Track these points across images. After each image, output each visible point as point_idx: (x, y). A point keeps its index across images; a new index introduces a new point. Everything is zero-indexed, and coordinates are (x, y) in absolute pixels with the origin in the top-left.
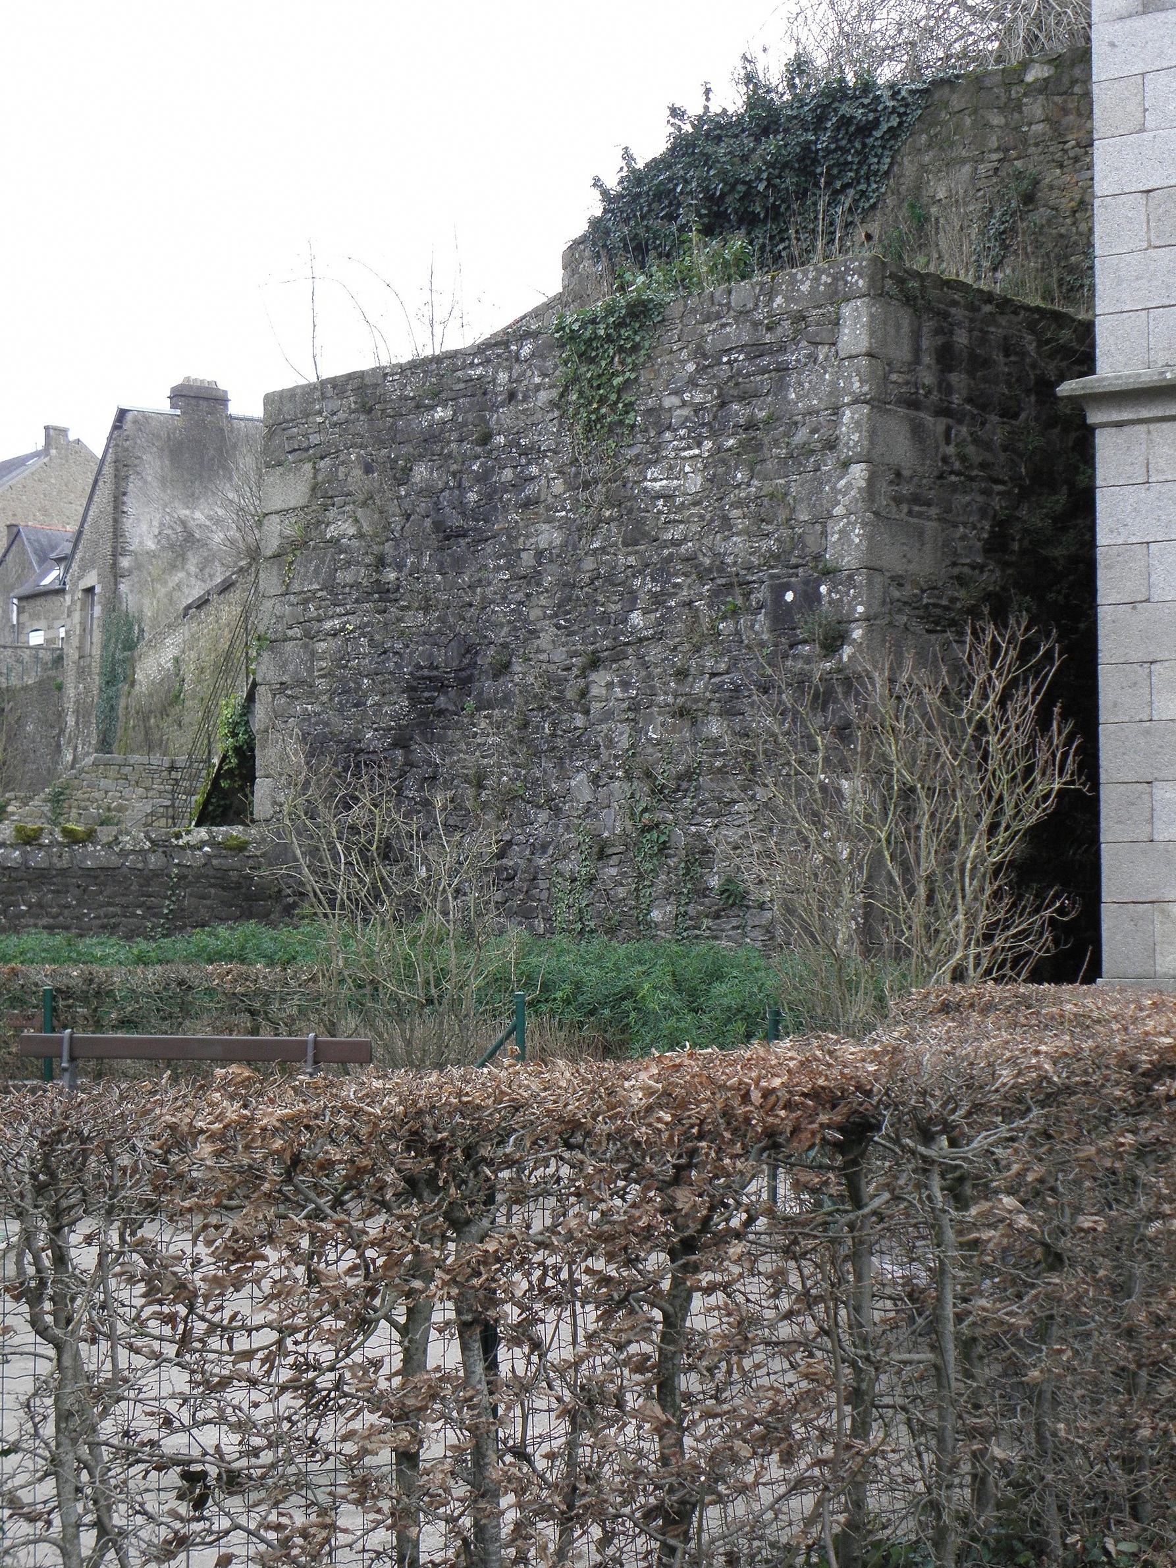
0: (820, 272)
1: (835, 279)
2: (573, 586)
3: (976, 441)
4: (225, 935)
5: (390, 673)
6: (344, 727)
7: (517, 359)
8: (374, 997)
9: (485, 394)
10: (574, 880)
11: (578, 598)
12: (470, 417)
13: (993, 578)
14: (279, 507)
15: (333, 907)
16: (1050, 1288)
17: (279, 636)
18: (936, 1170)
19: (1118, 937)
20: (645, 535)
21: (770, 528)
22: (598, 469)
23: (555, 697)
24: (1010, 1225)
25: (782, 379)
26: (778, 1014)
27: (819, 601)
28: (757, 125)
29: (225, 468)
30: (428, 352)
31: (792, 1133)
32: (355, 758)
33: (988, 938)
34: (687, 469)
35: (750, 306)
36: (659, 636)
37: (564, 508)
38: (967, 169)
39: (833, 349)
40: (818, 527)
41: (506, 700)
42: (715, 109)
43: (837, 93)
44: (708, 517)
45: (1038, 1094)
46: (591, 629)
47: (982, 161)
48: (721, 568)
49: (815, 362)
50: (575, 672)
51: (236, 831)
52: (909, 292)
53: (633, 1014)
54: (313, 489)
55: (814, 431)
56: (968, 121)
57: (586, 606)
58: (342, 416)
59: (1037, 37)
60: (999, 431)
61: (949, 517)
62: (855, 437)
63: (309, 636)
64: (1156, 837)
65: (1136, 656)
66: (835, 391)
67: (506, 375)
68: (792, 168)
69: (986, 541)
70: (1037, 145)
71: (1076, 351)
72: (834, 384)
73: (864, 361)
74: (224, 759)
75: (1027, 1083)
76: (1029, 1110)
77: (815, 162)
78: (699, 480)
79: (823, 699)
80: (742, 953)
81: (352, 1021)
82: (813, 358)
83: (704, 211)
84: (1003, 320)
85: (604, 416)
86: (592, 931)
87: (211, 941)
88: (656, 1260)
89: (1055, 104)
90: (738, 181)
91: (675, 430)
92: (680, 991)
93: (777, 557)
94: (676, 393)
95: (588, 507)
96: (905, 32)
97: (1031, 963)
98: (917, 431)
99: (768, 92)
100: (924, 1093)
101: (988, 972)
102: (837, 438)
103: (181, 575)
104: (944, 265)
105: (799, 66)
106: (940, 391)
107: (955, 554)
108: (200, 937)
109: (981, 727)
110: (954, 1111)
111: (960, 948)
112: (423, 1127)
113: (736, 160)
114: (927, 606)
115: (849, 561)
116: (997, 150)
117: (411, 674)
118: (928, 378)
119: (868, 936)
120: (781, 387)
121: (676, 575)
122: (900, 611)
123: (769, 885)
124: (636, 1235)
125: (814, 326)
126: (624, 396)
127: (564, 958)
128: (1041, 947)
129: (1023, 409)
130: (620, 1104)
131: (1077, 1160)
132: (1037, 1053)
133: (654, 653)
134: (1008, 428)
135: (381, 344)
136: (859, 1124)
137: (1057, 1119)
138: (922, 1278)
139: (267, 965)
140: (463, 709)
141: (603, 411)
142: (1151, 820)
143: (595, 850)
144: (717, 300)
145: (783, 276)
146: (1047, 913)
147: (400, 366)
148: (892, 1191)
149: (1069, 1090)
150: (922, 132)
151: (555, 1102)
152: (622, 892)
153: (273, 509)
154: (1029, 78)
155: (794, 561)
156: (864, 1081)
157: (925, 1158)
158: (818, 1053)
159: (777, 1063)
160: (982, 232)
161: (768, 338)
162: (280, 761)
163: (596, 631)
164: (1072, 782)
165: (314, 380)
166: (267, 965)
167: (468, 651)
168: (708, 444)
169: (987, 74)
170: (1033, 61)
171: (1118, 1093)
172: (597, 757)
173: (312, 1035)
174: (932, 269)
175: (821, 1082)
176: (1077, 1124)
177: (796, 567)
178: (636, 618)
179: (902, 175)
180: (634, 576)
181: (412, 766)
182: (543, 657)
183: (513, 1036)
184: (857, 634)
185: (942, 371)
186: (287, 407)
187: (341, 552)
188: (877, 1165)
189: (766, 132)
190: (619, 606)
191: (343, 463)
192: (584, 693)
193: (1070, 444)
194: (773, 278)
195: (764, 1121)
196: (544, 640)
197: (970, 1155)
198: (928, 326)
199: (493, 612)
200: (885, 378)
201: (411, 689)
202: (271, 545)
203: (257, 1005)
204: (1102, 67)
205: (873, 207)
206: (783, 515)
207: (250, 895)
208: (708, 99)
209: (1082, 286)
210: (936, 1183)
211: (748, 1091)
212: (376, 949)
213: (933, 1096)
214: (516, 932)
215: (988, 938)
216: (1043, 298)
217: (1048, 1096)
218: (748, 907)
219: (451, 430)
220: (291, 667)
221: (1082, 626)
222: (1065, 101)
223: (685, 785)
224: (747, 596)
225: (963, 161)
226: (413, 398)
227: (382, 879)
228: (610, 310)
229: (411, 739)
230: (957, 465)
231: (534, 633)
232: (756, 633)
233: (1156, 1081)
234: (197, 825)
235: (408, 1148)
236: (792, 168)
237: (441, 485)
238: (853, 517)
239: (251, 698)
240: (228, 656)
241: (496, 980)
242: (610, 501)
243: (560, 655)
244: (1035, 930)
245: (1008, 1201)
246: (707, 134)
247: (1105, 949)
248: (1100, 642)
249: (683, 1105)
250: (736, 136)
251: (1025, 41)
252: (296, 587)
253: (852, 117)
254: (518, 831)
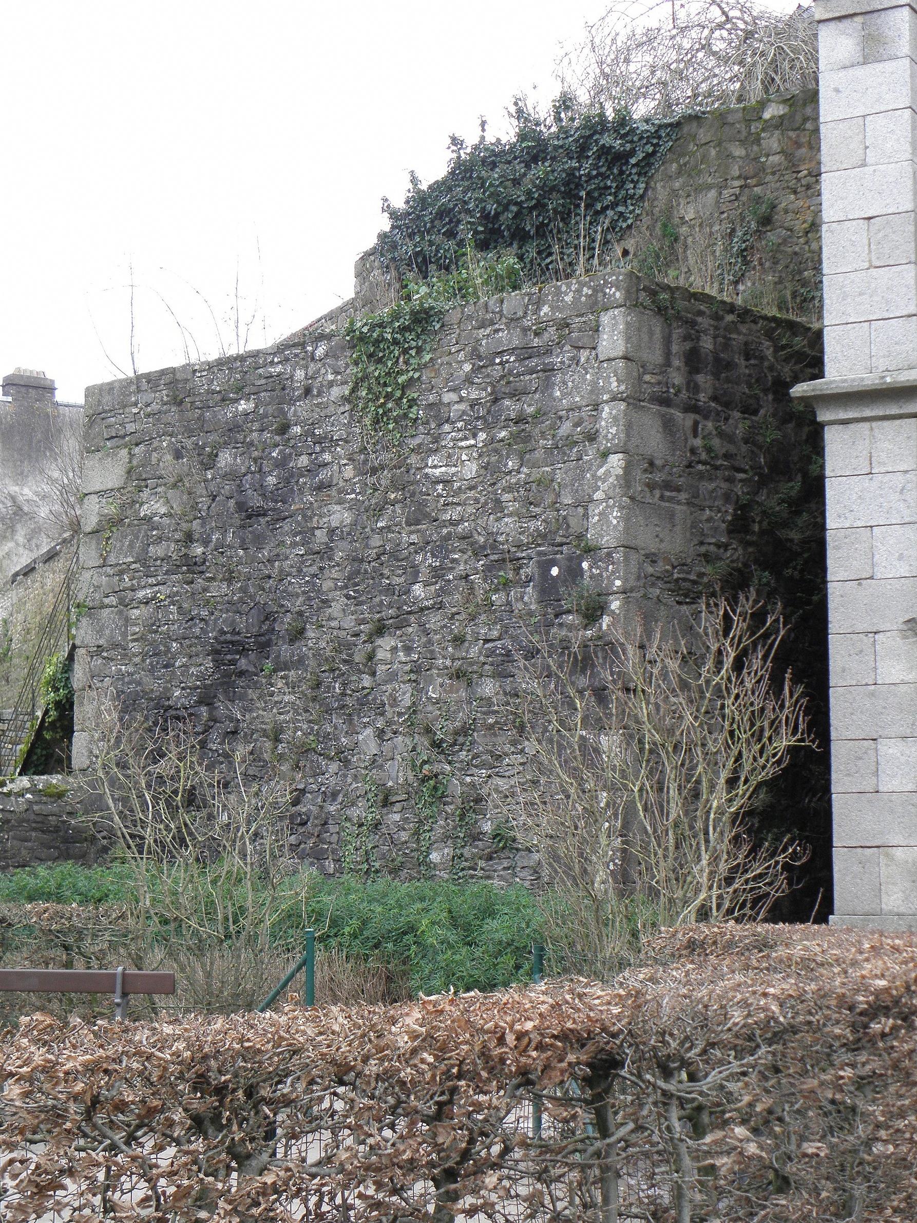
0: (582, 285)
1: (595, 291)
2: (362, 561)
3: (721, 434)
4: (44, 874)
5: (197, 637)
6: (155, 686)
7: (313, 359)
8: (178, 931)
9: (283, 389)
10: (361, 825)
11: (366, 571)
12: (270, 409)
13: (736, 555)
14: (97, 488)
15: (141, 853)
16: (777, 1209)
17: (97, 603)
18: (675, 1102)
19: (848, 879)
20: (427, 515)
21: (538, 510)
22: (385, 457)
23: (347, 659)
24: (741, 1153)
25: (548, 378)
26: (542, 949)
27: (582, 577)
28: (528, 153)
29: (51, 450)
30: (233, 351)
31: (542, 1071)
32: (165, 714)
33: (729, 881)
34: (464, 457)
35: (520, 314)
36: (440, 606)
37: (353, 491)
38: (713, 193)
39: (594, 353)
40: (580, 510)
41: (301, 662)
42: (490, 139)
43: (596, 126)
44: (482, 500)
45: (766, 1032)
46: (377, 600)
47: (726, 187)
48: (494, 545)
49: (577, 365)
50: (363, 637)
51: (55, 779)
52: (661, 304)
53: (414, 947)
54: (129, 472)
55: (577, 425)
56: (713, 152)
57: (373, 578)
58: (155, 407)
59: (773, 80)
60: (740, 426)
61: (696, 501)
62: (613, 430)
63: (124, 604)
64: (881, 789)
65: (860, 627)
66: (595, 390)
67: (303, 373)
68: (559, 191)
69: (731, 523)
70: (774, 173)
71: (808, 356)
72: (594, 383)
73: (621, 364)
74: (46, 713)
75: (756, 1023)
76: (758, 1046)
77: (579, 186)
78: (474, 467)
79: (584, 663)
80: (512, 892)
81: (159, 954)
82: (576, 360)
83: (481, 229)
84: (744, 329)
85: (390, 410)
86: (377, 871)
87: (32, 881)
88: (421, 1188)
89: (790, 138)
90: (510, 202)
91: (453, 423)
92: (455, 926)
93: (544, 536)
94: (454, 390)
95: (376, 490)
96: (658, 73)
97: (769, 903)
98: (668, 425)
99: (537, 124)
100: (663, 1034)
101: (730, 911)
102: (597, 431)
103: (11, 544)
104: (692, 279)
105: (564, 102)
106: (688, 390)
107: (702, 534)
108: (23, 877)
109: (719, 693)
110: (691, 1048)
111: (704, 889)
112: (208, 1070)
113: (509, 183)
114: (677, 580)
115: (608, 540)
116: (739, 177)
117: (215, 638)
118: (677, 379)
119: (623, 879)
120: (548, 385)
121: (454, 552)
122: (653, 585)
123: (534, 831)
124: (401, 1168)
125: (577, 333)
126: (408, 393)
127: (349, 896)
128: (779, 888)
129: (761, 407)
130: (387, 1047)
131: (801, 1091)
132: (765, 995)
133: (434, 621)
134: (748, 422)
135: (190, 343)
136: (606, 1061)
137: (784, 1055)
138: (666, 1197)
139: (80, 903)
140: (262, 670)
141: (390, 405)
142: (876, 773)
143: (381, 797)
144: (491, 309)
145: (549, 288)
146: (780, 858)
147: (208, 363)
148: (636, 1121)
149: (793, 1029)
150: (672, 161)
151: (329, 1046)
152: (404, 836)
153: (92, 490)
154: (767, 115)
155: (559, 540)
156: (608, 1024)
157: (665, 1093)
158: (568, 997)
159: (532, 1004)
160: (725, 250)
161: (536, 342)
162: (95, 714)
163: (381, 601)
164: (802, 740)
165: (131, 374)
166: (80, 903)
167: (267, 619)
168: (482, 436)
169: (730, 111)
170: (769, 100)
171: (837, 1031)
172: (382, 714)
173: (120, 969)
174: (682, 282)
175: (569, 1025)
176: (802, 1059)
177: (561, 545)
178: (418, 590)
179: (656, 199)
180: (416, 552)
181: (216, 721)
182: (334, 624)
183: (304, 968)
184: (615, 605)
185: (690, 373)
186: (107, 399)
187: (153, 529)
188: (622, 1098)
189: (535, 159)
190: (402, 579)
191: (155, 450)
192: (371, 657)
193: (804, 437)
194: (540, 290)
195: (517, 1061)
196: (335, 609)
197: (705, 1089)
198: (678, 332)
199: (290, 583)
200: (640, 378)
201: (216, 652)
202: (91, 522)
203: (71, 940)
204: (830, 109)
205: (629, 227)
206: (549, 499)
207: (66, 839)
208: (483, 130)
209: (813, 298)
210: (675, 1113)
211: (504, 1034)
212: (180, 890)
213: (671, 1035)
214: (308, 873)
215: (729, 881)
216: (780, 309)
217: (775, 1034)
218: (518, 850)
219: (252, 421)
220: (107, 632)
221: (815, 598)
222: (798, 136)
223: (461, 739)
224: (517, 570)
225: (709, 187)
226: (220, 392)
227: (186, 825)
228: (396, 316)
229: (215, 697)
230: (704, 456)
231: (326, 603)
232: (525, 604)
233: (872, 1020)
234: (20, 774)
235: (195, 1089)
236: (559, 191)
237: (243, 470)
238: (611, 502)
239: (71, 657)
240: (52, 618)
241: (290, 916)
242: (395, 485)
243: (349, 622)
244: (771, 872)
245: (740, 1131)
246: (483, 161)
247: (836, 888)
248: (830, 614)
249: (443, 1048)
250: (509, 162)
251: (763, 82)
252: (112, 560)
253: (611, 147)
254: (311, 780)
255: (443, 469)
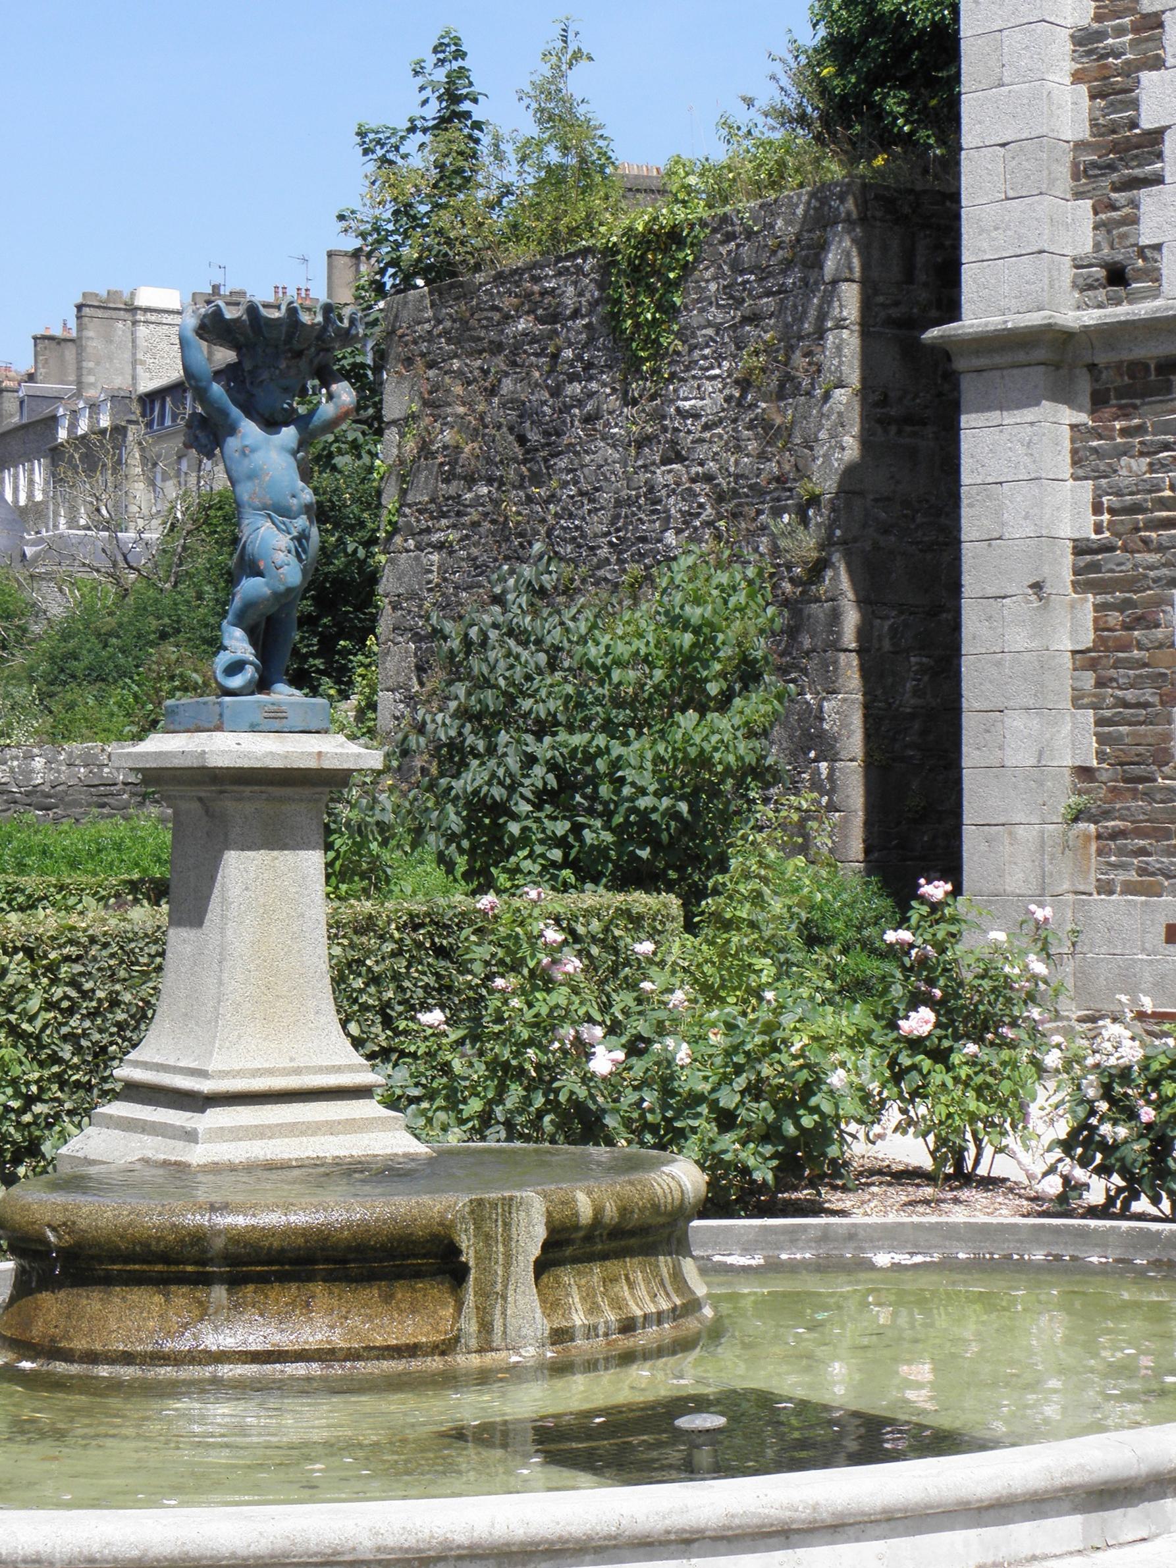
64: (1007, 764)
65: (991, 591)
255: (693, 402)
